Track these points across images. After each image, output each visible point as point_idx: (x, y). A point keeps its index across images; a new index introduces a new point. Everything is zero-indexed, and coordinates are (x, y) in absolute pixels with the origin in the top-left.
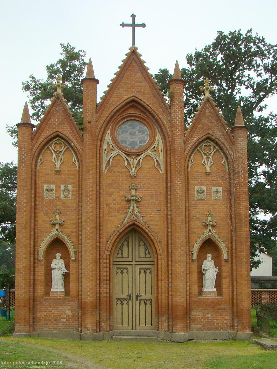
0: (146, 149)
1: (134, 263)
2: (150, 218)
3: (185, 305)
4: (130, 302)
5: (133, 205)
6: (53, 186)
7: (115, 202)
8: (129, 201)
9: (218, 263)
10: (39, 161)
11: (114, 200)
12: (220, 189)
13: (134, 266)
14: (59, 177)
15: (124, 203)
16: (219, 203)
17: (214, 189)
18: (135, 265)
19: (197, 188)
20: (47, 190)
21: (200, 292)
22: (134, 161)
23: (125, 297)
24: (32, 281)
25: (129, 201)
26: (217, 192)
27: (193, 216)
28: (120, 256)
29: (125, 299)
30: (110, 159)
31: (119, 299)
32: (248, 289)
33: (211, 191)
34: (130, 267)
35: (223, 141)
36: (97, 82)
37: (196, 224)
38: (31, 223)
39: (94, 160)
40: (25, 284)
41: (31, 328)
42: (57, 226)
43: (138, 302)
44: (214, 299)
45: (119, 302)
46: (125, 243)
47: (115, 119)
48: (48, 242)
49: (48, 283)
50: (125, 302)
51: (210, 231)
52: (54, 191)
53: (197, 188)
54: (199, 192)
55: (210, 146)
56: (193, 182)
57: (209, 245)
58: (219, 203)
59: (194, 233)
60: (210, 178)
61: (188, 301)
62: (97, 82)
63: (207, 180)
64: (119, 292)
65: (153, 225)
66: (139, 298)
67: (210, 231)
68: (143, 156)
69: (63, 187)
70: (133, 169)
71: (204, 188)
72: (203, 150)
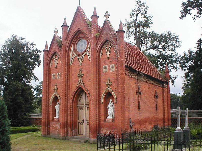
0: (85, 52)
1: (85, 105)
2: (86, 84)
3: (96, 126)
4: (83, 123)
5: (80, 78)
6: (55, 74)
7: (74, 78)
8: (79, 77)
9: (115, 103)
10: (100, 54)
11: (74, 77)
12: (114, 65)
13: (85, 107)
14: (56, 70)
15: (77, 78)
16: (113, 73)
17: (111, 66)
18: (85, 106)
19: (104, 66)
20: (104, 68)
21: (105, 120)
22: (80, 58)
23: (81, 121)
24: (47, 114)
25: (79, 77)
26: (112, 67)
27: (102, 81)
28: (80, 102)
29: (82, 122)
30: (82, 57)
31: (80, 122)
32: (121, 118)
33: (110, 67)
34: (83, 107)
35: (113, 40)
36: (98, 17)
37: (103, 85)
38: (46, 90)
39: (64, 61)
40: (44, 115)
41: (47, 133)
42: (56, 90)
43: (86, 124)
44: (110, 123)
45: (80, 123)
46: (82, 96)
47: (74, 40)
48: (53, 98)
49: (106, 114)
50: (82, 124)
51: (108, 88)
52: (107, 68)
53: (104, 66)
54: (54, 76)
55: (109, 44)
56: (102, 64)
57: (109, 95)
58: (113, 73)
59: (103, 89)
60: (109, 61)
61: (98, 124)
62: (98, 17)
63: (108, 62)
64: (80, 119)
65: (88, 87)
66: (87, 122)
67: (108, 88)
68: (84, 55)
69: (58, 74)
70: (80, 62)
71: (107, 66)
72: (106, 47)
